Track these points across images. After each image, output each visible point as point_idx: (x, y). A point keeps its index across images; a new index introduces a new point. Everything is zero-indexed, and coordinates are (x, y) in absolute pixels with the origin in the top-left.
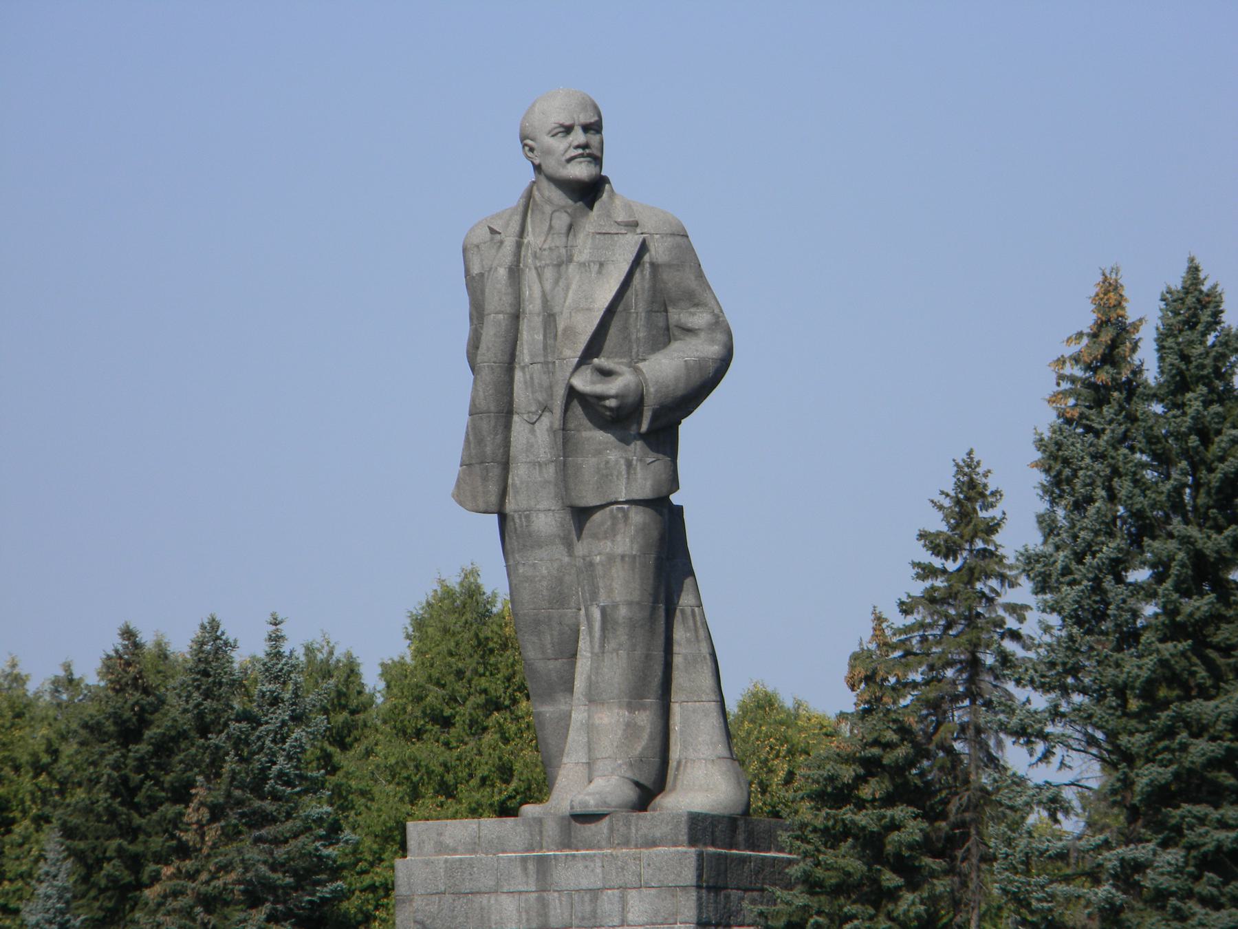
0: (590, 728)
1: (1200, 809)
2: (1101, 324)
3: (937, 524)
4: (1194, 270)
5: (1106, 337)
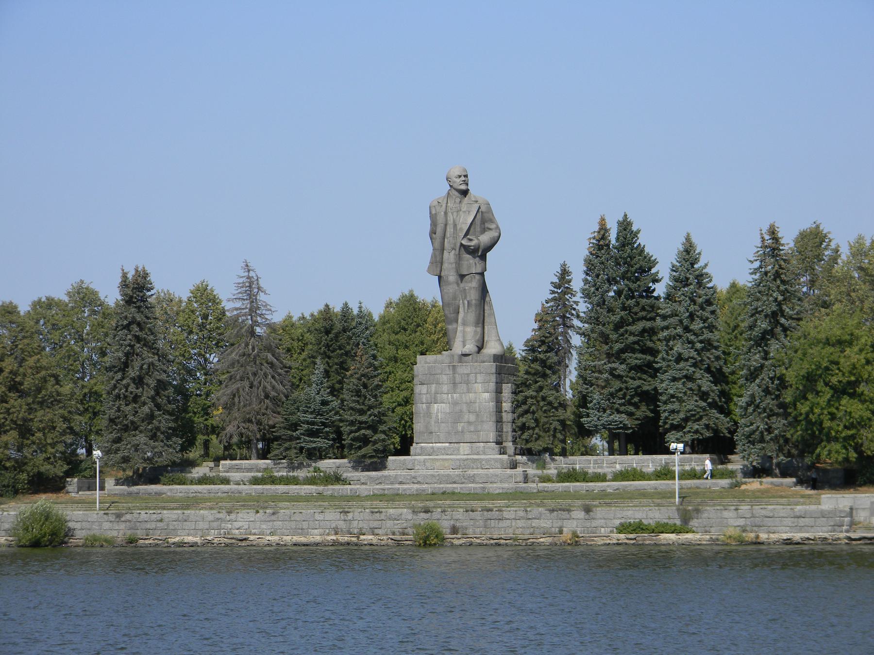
0: (464, 332)
1: (630, 355)
2: (601, 229)
3: (556, 280)
4: (626, 215)
5: (602, 233)
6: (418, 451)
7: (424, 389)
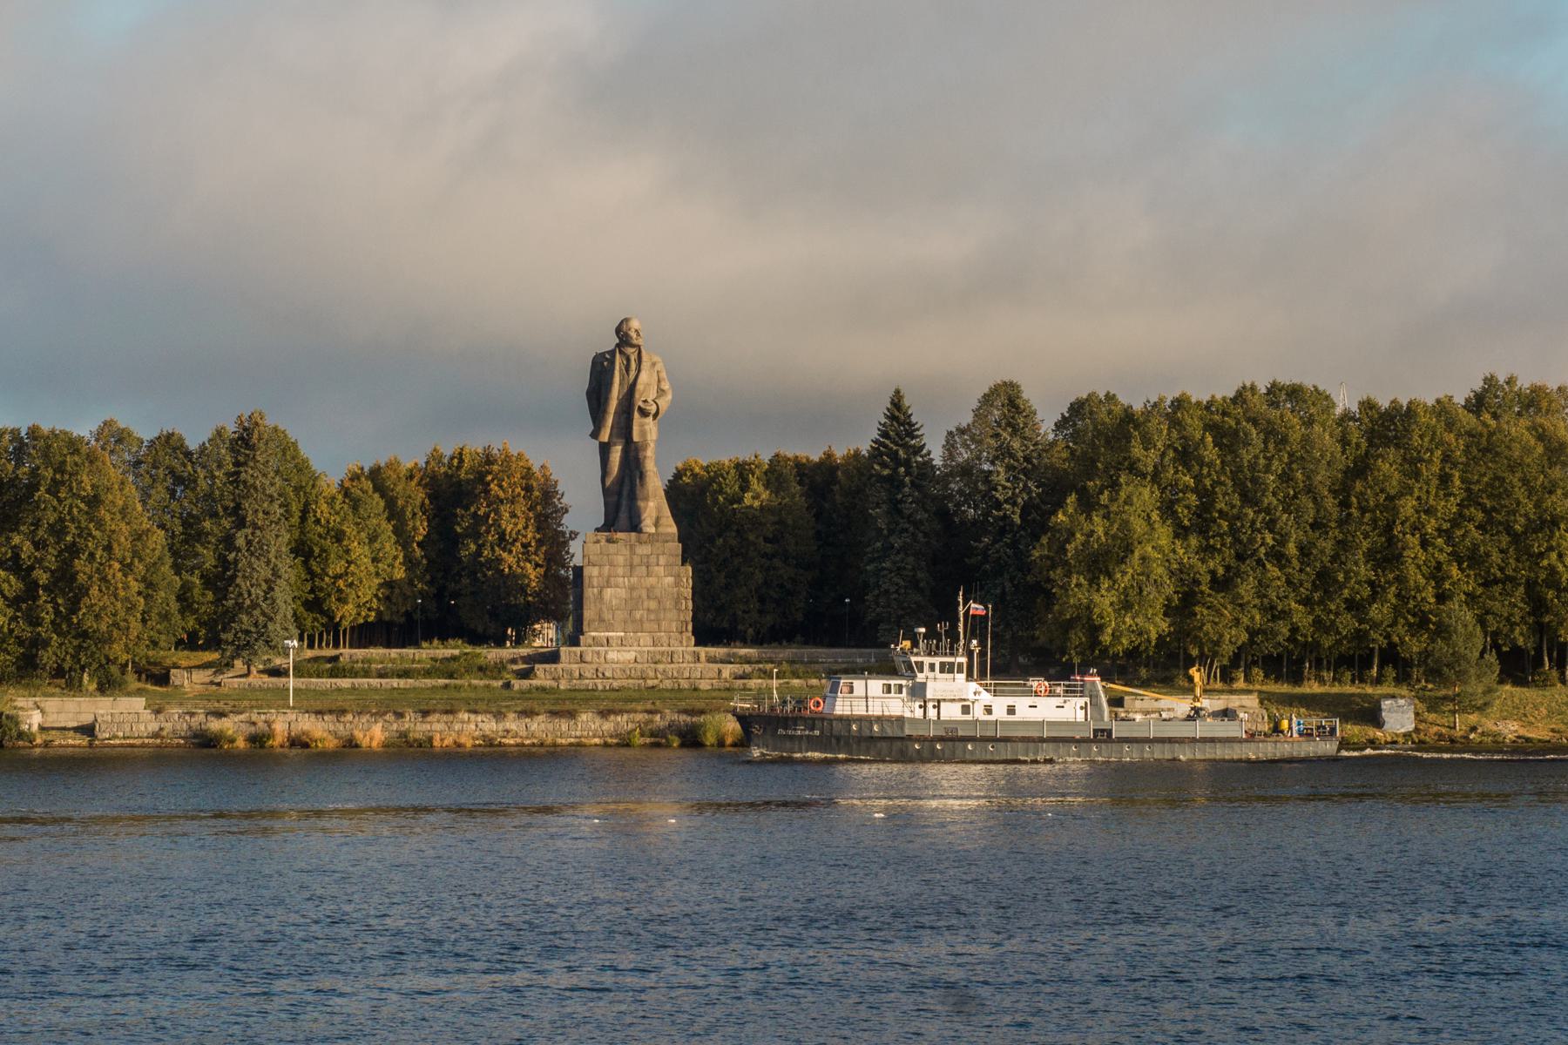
6: (590, 641)
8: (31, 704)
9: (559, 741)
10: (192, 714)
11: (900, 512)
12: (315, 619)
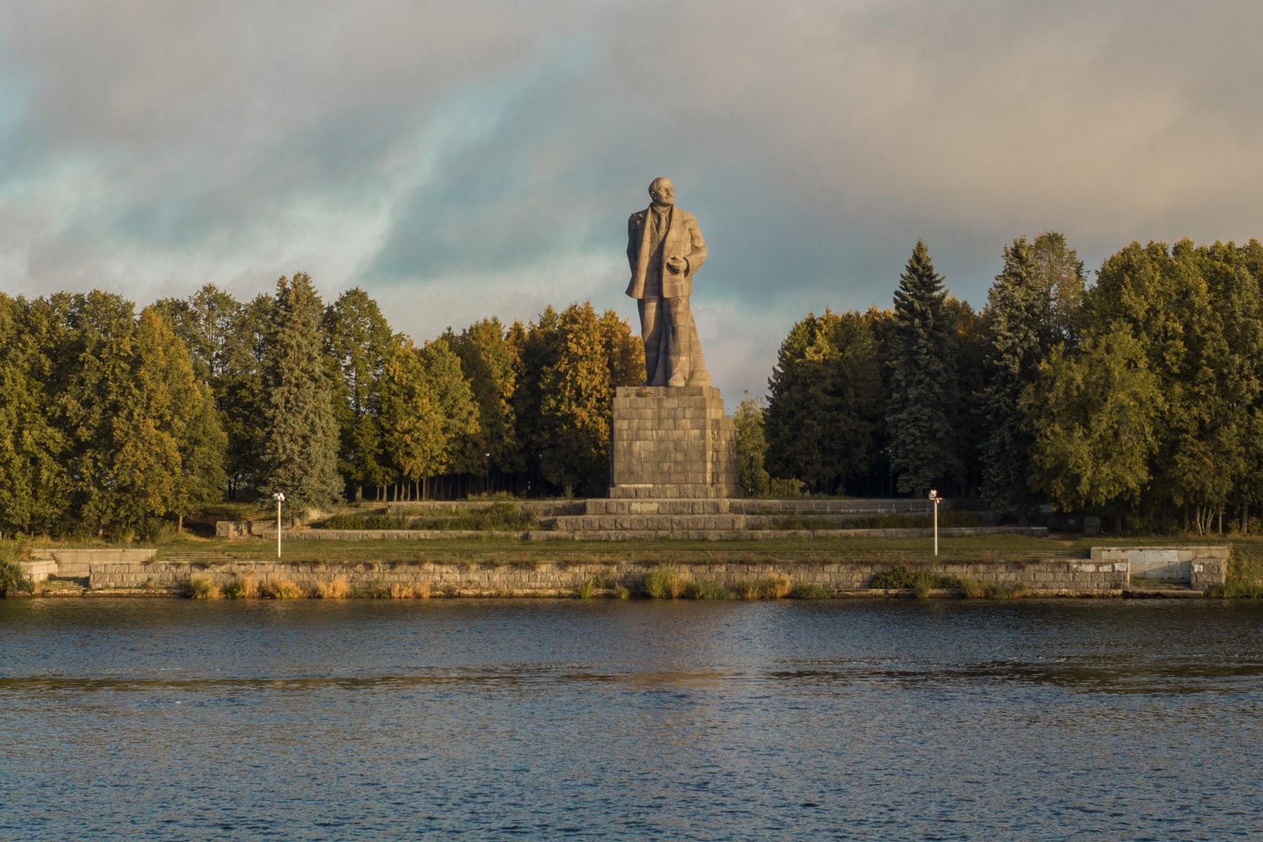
6: (620, 493)
7: (625, 425)
8: (48, 555)
9: (518, 592)
10: (178, 565)
11: (917, 364)
12: (387, 473)
